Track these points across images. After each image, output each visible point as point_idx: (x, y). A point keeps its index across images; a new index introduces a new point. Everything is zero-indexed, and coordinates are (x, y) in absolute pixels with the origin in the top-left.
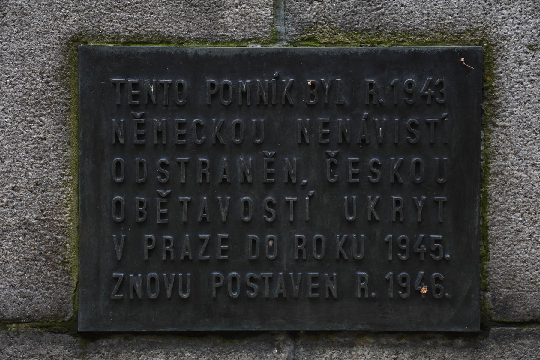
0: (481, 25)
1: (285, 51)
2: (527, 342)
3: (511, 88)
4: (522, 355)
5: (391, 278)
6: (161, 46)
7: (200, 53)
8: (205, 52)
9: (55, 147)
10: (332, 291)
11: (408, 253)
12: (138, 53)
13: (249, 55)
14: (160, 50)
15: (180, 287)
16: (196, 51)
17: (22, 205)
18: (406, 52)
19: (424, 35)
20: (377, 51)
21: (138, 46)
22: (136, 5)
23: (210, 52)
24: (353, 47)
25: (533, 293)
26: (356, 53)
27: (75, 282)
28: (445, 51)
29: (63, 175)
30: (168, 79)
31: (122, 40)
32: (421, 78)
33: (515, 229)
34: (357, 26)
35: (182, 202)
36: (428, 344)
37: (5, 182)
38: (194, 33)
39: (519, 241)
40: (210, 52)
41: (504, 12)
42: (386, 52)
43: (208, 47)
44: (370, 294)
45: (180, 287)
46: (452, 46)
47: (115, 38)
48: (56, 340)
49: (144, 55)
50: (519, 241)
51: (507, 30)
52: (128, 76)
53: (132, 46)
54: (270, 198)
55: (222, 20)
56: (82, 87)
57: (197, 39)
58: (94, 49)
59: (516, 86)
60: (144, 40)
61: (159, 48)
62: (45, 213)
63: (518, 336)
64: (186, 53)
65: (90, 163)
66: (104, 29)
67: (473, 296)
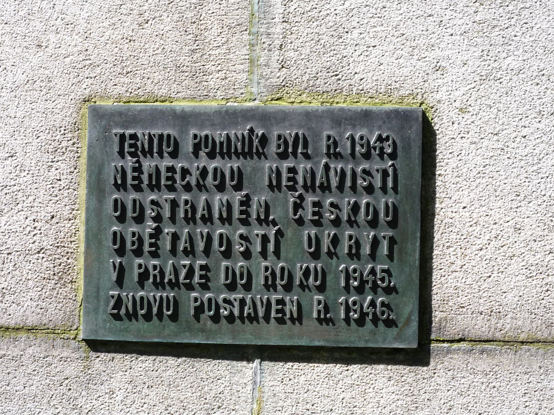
0: (420, 90)
1: (257, 108)
2: (456, 356)
3: (446, 143)
4: (452, 368)
5: (344, 301)
6: (155, 104)
7: (186, 110)
8: (191, 109)
9: (68, 187)
10: (293, 311)
11: (358, 279)
12: (135, 110)
13: (227, 111)
14: (154, 108)
15: (165, 305)
16: (183, 108)
17: (41, 233)
18: (359, 110)
19: (373, 98)
20: (334, 109)
21: (137, 104)
22: (136, 72)
23: (194, 109)
24: (315, 105)
25: (463, 316)
26: (317, 111)
27: (81, 298)
28: (391, 111)
29: (73, 210)
30: (159, 130)
31: (124, 100)
32: (371, 132)
33: (449, 261)
34: (318, 89)
35: (257, 235)
36: (375, 358)
37: (29, 215)
38: (183, 94)
39: (452, 272)
40: (194, 109)
41: (439, 81)
42: (342, 110)
43: (192, 104)
44: (325, 315)
45: (165, 305)
46: (397, 106)
47: (119, 99)
48: (65, 345)
49: (141, 111)
50: (452, 272)
51: (442, 95)
52: (127, 129)
53: (132, 104)
54: (353, 266)
55: (206, 83)
56: (89, 138)
57: (184, 98)
58: (101, 107)
59: (450, 142)
60: (142, 99)
61: (153, 106)
62: (58, 241)
63: (449, 351)
64: (175, 110)
65: (94, 200)
66: (110, 91)
67: (413, 318)
